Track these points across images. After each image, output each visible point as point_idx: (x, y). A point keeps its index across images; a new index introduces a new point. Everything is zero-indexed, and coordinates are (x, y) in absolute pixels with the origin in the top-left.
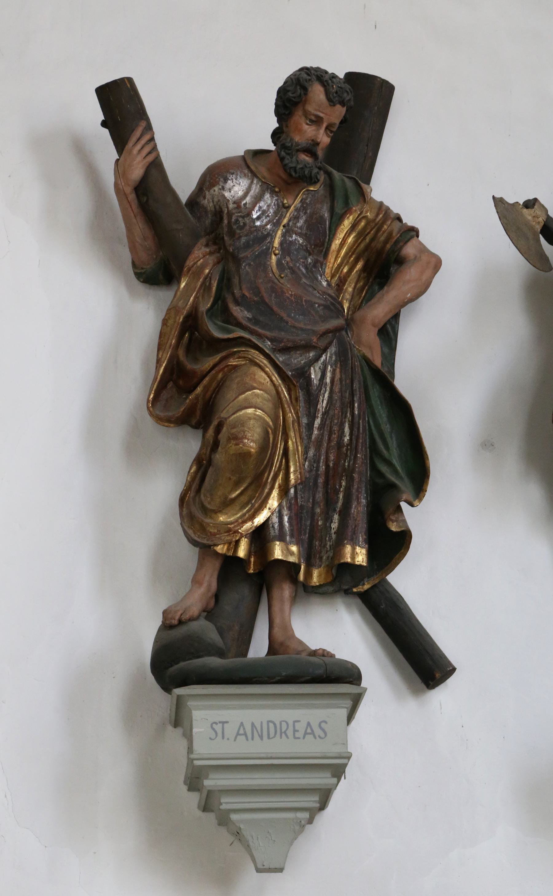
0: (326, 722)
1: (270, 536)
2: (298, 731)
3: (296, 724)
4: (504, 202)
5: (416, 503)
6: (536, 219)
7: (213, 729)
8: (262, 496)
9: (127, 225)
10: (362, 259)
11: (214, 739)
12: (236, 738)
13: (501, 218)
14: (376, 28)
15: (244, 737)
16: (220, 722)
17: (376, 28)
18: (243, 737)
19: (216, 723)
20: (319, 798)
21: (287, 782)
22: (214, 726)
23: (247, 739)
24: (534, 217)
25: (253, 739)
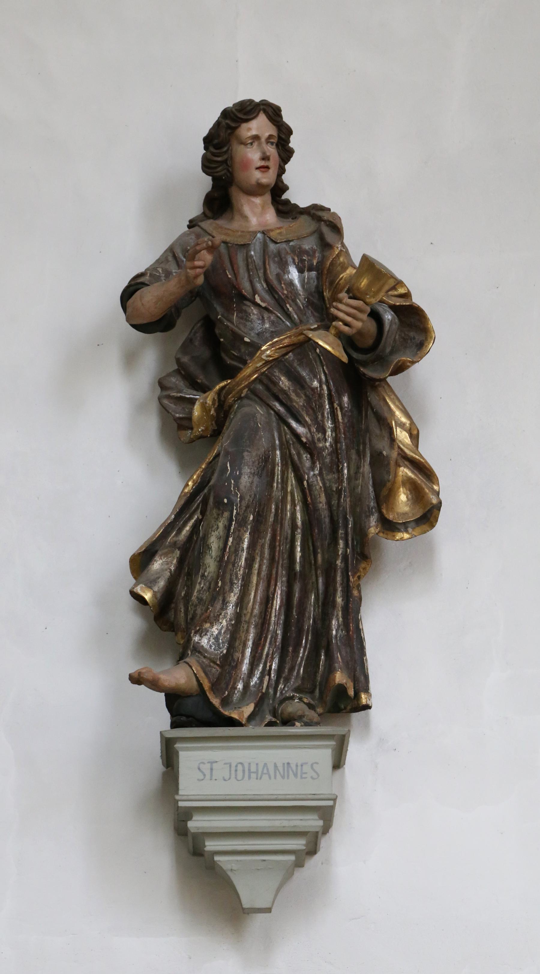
0: (317, 763)
1: (385, 385)
8: (277, 311)
11: (238, 780)
15: (267, 775)
16: (209, 762)
19: (203, 763)
20: (306, 842)
21: (286, 823)
23: (270, 778)
25: (275, 778)
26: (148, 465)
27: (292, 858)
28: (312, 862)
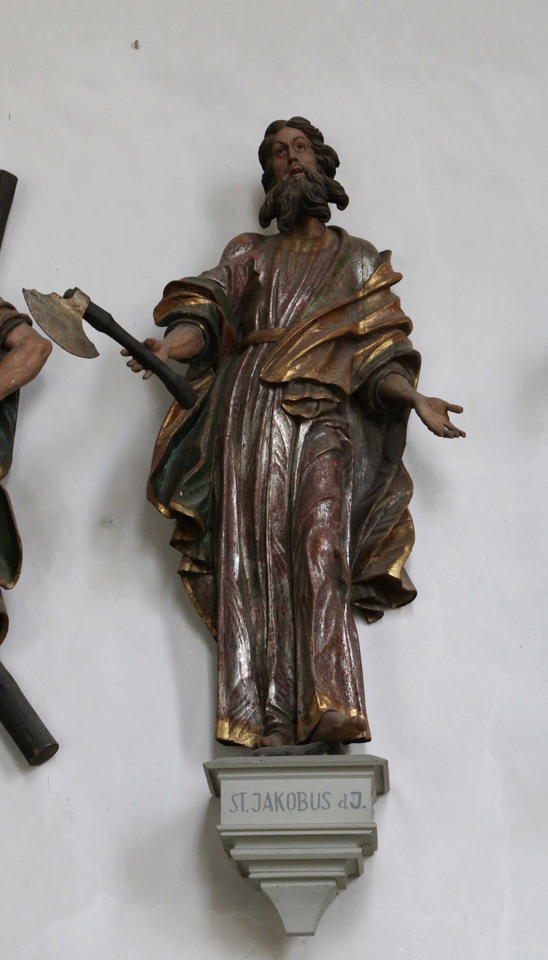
0: (329, 793)
4: (37, 294)
5: (10, 586)
6: (76, 308)
7: (327, 801)
12: (264, 809)
13: (31, 310)
14: (9, 119)
17: (9, 119)
18: (269, 809)
19: (237, 795)
23: (283, 809)
24: (74, 306)
25: (277, 810)
26: (4, 258)
27: (332, 884)
28: (353, 886)
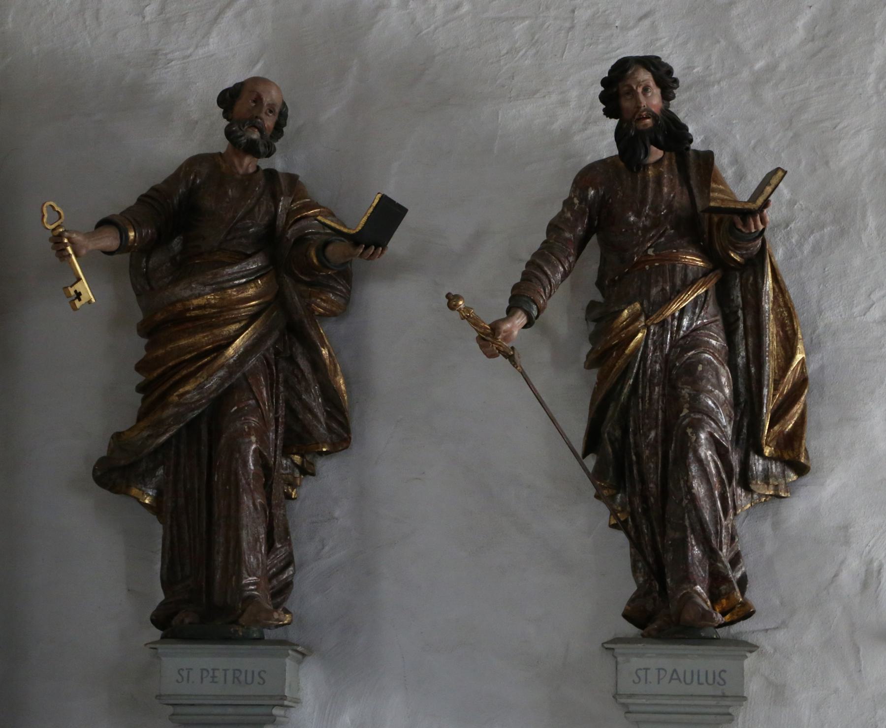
2: (216, 677)
3: (638, 671)
9: (70, 263)
10: (163, 466)
11: (636, 683)
22: (181, 671)
